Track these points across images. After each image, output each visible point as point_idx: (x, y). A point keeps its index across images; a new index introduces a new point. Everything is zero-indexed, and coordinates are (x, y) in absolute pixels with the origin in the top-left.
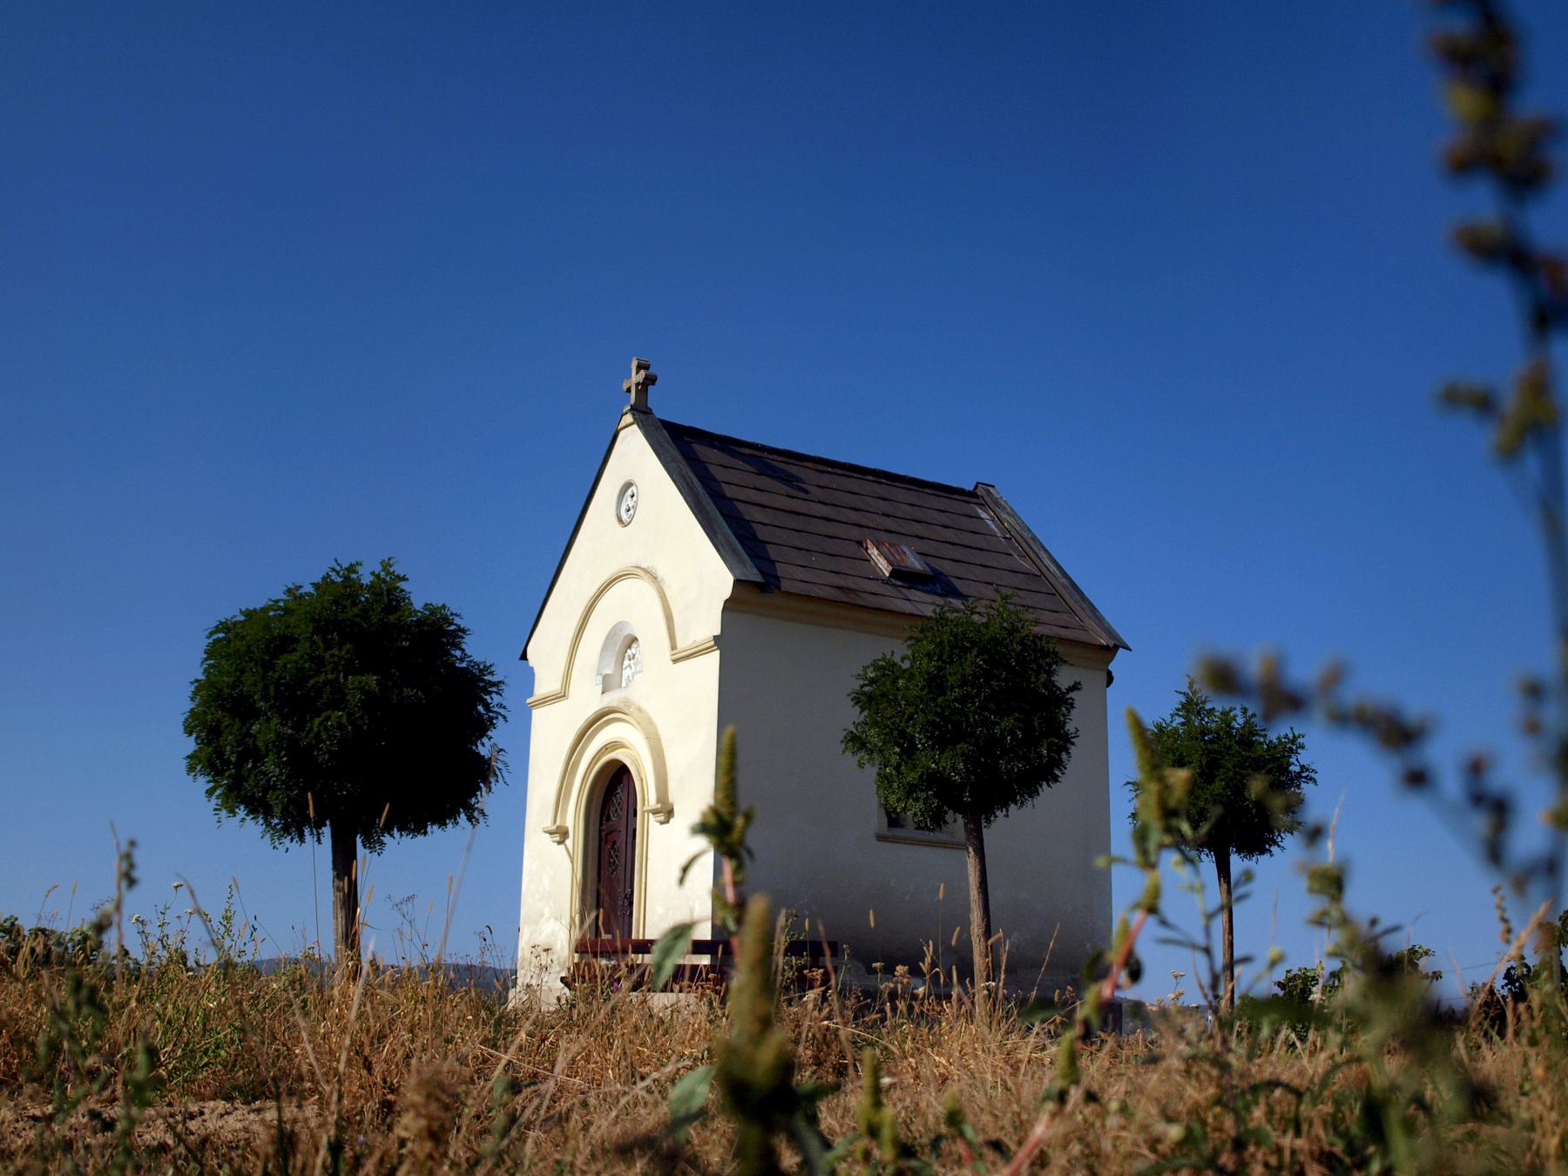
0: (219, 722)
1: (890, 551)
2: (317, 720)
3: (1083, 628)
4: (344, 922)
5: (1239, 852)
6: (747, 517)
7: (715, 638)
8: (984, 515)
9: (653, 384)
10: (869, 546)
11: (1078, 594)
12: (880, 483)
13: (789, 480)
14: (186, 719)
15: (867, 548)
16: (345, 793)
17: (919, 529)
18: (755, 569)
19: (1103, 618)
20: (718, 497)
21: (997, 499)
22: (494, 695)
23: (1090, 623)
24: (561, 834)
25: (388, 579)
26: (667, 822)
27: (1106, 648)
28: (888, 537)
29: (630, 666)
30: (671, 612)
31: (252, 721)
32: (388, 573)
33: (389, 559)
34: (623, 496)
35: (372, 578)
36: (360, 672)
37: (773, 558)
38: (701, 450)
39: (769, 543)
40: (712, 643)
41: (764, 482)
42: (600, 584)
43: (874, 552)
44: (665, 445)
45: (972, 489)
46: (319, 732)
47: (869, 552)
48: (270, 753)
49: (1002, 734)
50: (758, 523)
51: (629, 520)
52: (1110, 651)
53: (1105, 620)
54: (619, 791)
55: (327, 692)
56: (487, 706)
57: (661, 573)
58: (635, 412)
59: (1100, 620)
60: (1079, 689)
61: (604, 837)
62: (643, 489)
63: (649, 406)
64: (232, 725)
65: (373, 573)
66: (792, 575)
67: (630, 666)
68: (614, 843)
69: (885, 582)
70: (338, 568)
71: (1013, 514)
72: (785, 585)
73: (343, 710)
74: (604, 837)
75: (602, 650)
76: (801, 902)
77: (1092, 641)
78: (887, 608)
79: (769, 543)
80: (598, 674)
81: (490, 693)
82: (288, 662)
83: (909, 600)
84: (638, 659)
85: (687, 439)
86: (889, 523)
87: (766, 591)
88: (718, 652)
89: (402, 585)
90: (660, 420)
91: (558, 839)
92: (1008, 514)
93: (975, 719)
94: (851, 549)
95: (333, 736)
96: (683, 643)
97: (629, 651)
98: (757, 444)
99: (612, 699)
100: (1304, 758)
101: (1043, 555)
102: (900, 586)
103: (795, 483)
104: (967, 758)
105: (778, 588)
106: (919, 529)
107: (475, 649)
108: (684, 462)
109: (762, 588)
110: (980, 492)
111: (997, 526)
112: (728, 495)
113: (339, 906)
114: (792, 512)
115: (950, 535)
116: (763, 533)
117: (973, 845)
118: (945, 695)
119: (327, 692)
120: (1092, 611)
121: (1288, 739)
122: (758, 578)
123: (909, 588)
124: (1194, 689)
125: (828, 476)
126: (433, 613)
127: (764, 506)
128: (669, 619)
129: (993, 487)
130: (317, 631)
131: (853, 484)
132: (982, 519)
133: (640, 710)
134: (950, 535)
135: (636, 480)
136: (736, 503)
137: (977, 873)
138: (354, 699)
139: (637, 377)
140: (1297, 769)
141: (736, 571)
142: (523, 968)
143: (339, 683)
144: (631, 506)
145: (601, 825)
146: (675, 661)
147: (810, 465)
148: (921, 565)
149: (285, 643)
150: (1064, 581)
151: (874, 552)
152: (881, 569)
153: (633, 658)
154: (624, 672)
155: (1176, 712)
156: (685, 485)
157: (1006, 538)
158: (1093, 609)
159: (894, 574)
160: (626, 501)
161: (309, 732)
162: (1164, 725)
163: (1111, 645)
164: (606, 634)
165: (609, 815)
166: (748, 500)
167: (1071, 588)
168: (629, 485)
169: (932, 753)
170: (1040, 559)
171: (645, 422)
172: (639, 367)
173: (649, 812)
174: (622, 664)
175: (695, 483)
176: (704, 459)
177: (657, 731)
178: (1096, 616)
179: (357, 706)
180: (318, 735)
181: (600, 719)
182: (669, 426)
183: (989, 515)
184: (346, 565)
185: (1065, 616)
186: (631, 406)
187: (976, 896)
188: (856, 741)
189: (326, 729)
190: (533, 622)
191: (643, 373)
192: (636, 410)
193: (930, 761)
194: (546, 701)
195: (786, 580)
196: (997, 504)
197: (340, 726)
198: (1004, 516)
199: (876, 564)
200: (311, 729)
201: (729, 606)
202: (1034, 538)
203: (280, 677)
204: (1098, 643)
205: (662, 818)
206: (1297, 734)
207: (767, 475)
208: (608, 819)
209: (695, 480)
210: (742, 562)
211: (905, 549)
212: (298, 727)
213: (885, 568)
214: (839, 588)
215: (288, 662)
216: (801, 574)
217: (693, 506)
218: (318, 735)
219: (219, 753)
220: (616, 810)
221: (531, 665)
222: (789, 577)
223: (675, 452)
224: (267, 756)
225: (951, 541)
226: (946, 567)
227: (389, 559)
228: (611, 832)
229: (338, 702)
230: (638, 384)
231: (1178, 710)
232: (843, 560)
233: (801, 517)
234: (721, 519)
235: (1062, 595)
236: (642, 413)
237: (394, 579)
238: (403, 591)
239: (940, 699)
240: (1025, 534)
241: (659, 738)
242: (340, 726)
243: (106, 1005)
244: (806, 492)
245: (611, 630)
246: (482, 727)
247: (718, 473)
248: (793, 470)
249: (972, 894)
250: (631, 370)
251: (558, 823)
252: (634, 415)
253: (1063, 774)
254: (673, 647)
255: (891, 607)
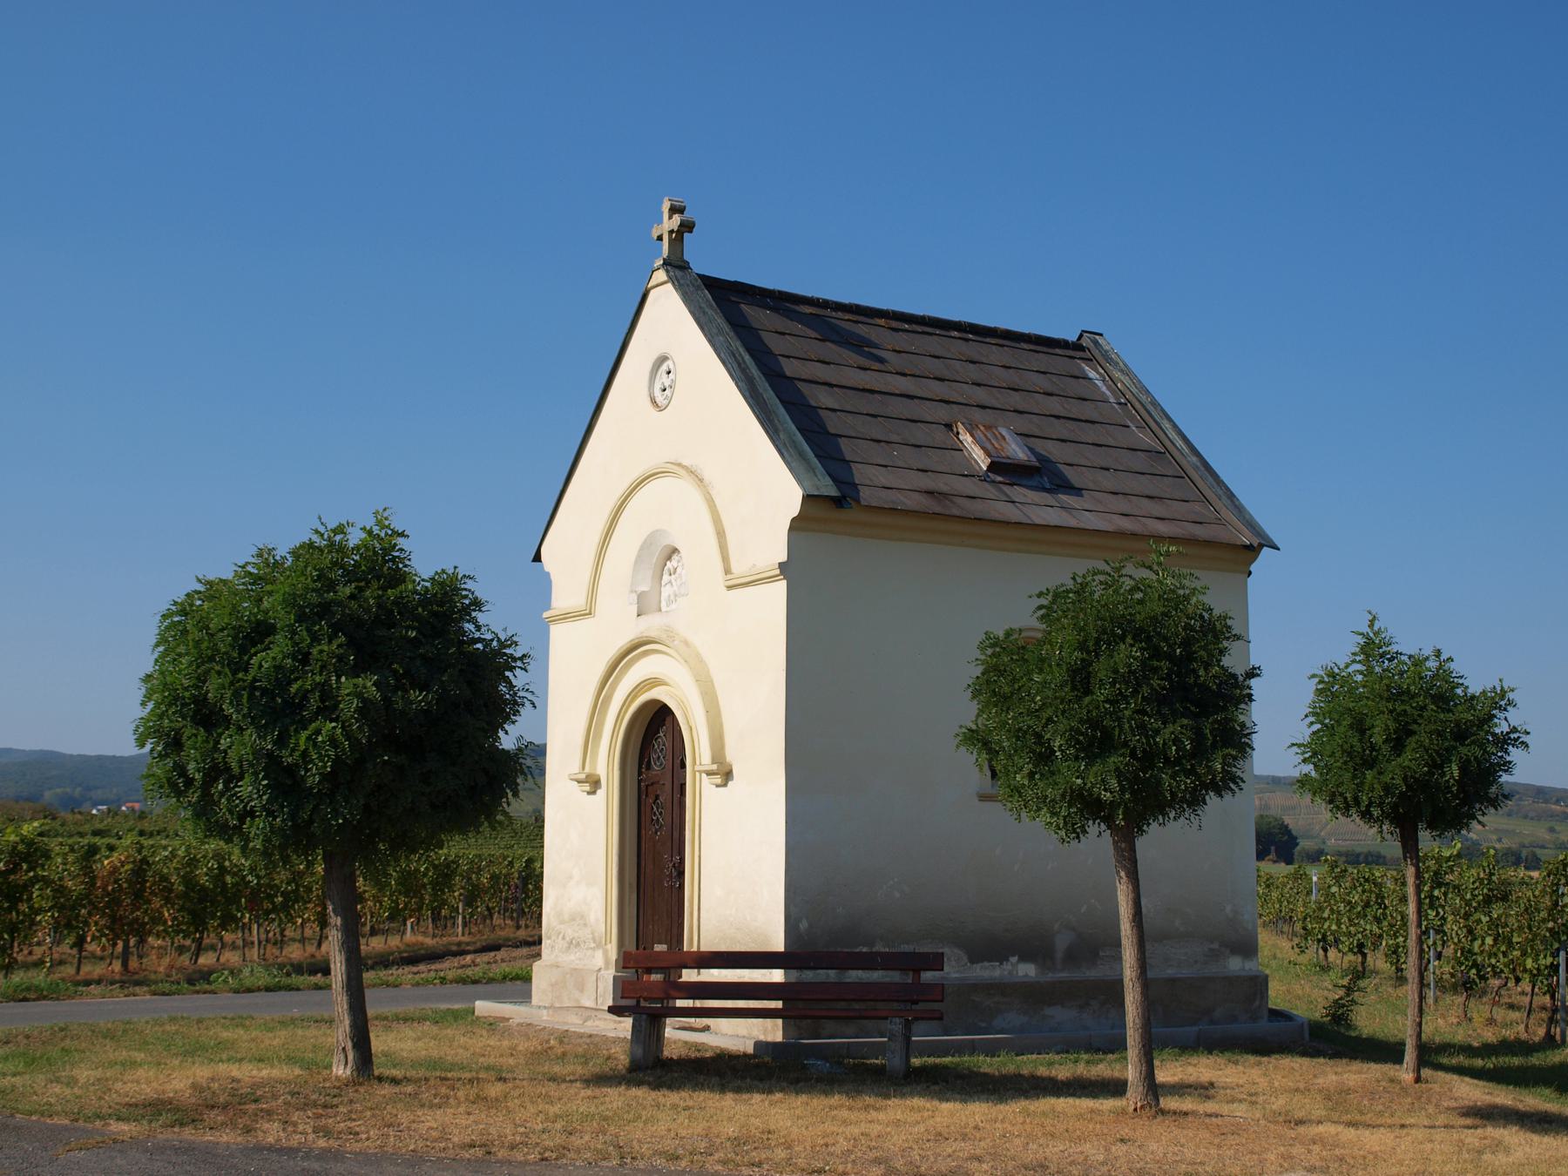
0: (178, 733)
1: (985, 435)
2: (304, 735)
3: (1220, 522)
4: (343, 968)
5: (1431, 826)
6: (813, 403)
7: (781, 565)
8: (1092, 374)
9: (691, 231)
10: (961, 431)
11: (1212, 476)
12: (967, 340)
13: (859, 345)
14: (137, 727)
15: (958, 433)
16: (341, 821)
17: (1016, 400)
18: (828, 478)
19: (1243, 507)
20: (775, 376)
21: (1106, 351)
22: (518, 672)
23: (1228, 515)
24: (594, 784)
25: (383, 535)
26: (725, 785)
27: (1249, 548)
28: (984, 415)
29: (670, 582)
30: (722, 526)
31: (220, 731)
32: (383, 527)
33: (385, 510)
34: (657, 370)
35: (363, 535)
36: (355, 672)
37: (848, 458)
38: (750, 311)
39: (841, 436)
40: (778, 572)
41: (831, 350)
42: (631, 481)
43: (966, 438)
44: (710, 312)
45: (1075, 340)
46: (307, 749)
47: (961, 437)
48: (246, 775)
49: (1164, 744)
50: (826, 409)
51: (666, 402)
52: (1252, 551)
53: (1245, 509)
54: (661, 734)
55: (314, 701)
56: (511, 686)
57: (707, 476)
58: (669, 268)
59: (1239, 509)
60: (1258, 675)
61: (643, 788)
62: (679, 361)
63: (686, 257)
64: (196, 736)
65: (363, 529)
66: (871, 478)
67: (670, 582)
68: (657, 797)
69: (984, 478)
70: (322, 530)
71: (1127, 372)
72: (865, 494)
73: (336, 720)
74: (643, 788)
75: (636, 562)
76: (891, 882)
77: (1232, 541)
78: (987, 516)
79: (841, 436)
80: (632, 592)
81: (512, 669)
82: (264, 661)
83: (1013, 502)
84: (680, 574)
85: (733, 299)
86: (981, 395)
87: (842, 507)
88: (785, 582)
89: (401, 542)
90: (702, 277)
91: (588, 789)
92: (1122, 371)
93: (1131, 726)
94: (939, 435)
95: (326, 756)
96: (740, 568)
97: (668, 563)
98: (818, 299)
99: (649, 625)
100: (1514, 717)
101: (1166, 425)
102: (1000, 482)
103: (866, 349)
104: (1119, 774)
105: (858, 501)
106: (1016, 400)
107: (493, 622)
108: (732, 334)
109: (838, 502)
110: (1085, 342)
111: (1108, 388)
112: (788, 373)
113: (337, 948)
114: (864, 390)
115: (1054, 405)
116: (833, 424)
117: (1124, 868)
118: (1093, 693)
119: (314, 701)
120: (1229, 498)
121: (1496, 693)
122: (833, 491)
123: (1012, 485)
124: (1376, 628)
125: (904, 335)
126: (442, 584)
127: (831, 385)
128: (721, 534)
129: (1101, 335)
130: (301, 618)
131: (933, 344)
132: (1090, 379)
133: (686, 643)
134: (1054, 405)
135: (672, 353)
136: (800, 385)
137: (1130, 902)
138: (349, 707)
139: (670, 223)
140: (1506, 729)
141: (806, 484)
142: (549, 938)
143: (331, 685)
144: (667, 385)
145: (640, 774)
146: (730, 588)
147: (882, 322)
148: (1023, 452)
149: (259, 633)
150: (1194, 459)
151: (966, 438)
152: (975, 461)
153: (675, 573)
154: (663, 589)
155: (1353, 658)
156: (735, 366)
157: (1120, 404)
158: (1231, 496)
159: (993, 467)
160: (661, 378)
161: (293, 750)
162: (1336, 670)
163: (1255, 545)
164: (640, 544)
165: (649, 762)
166: (811, 378)
167: (1203, 469)
168: (663, 359)
169: (1077, 765)
170: (1163, 430)
171: (682, 282)
172: (674, 210)
173: (700, 772)
174: (661, 579)
175: (748, 362)
176: (755, 325)
177: (708, 671)
178: (1236, 506)
179: (352, 717)
180: (305, 754)
181: (635, 649)
182: (711, 284)
183: (1098, 373)
184: (332, 525)
185: (1197, 507)
186: (664, 259)
187: (1129, 932)
188: (976, 738)
189: (315, 744)
190: (548, 518)
191: (677, 219)
192: (670, 265)
193: (1072, 775)
194: (566, 617)
195: (859, 466)
196: (1109, 360)
197: (333, 742)
198: (1117, 374)
199: (970, 454)
200: (297, 744)
201: (797, 525)
202: (1155, 403)
203: (255, 680)
204: (1238, 543)
205: (719, 781)
206: (1506, 688)
207: (833, 342)
208: (649, 767)
209: (747, 357)
210: (812, 470)
211: (1004, 431)
212: (281, 741)
213: (983, 462)
214: (930, 493)
215: (264, 661)
216: (882, 476)
217: (747, 394)
218: (305, 754)
219: (181, 770)
220: (659, 757)
221: (546, 569)
222: (868, 482)
223: (720, 320)
224: (241, 778)
225: (1057, 414)
226: (1054, 451)
227: (385, 510)
228: (652, 784)
229: (329, 707)
230: (671, 232)
231: (1354, 654)
232: (930, 452)
233: (876, 396)
234: (782, 411)
235: (1193, 479)
236: (677, 266)
237: (390, 536)
238: (401, 550)
239: (1087, 700)
240: (1143, 398)
241: (712, 681)
242: (333, 742)
243: (52, 1124)
244: (881, 360)
245: (646, 540)
246: (502, 709)
247: (775, 344)
248: (862, 330)
249: (1122, 928)
250: (662, 213)
251: (587, 770)
252: (667, 271)
253: (1241, 789)
254: (727, 571)
255: (995, 515)
